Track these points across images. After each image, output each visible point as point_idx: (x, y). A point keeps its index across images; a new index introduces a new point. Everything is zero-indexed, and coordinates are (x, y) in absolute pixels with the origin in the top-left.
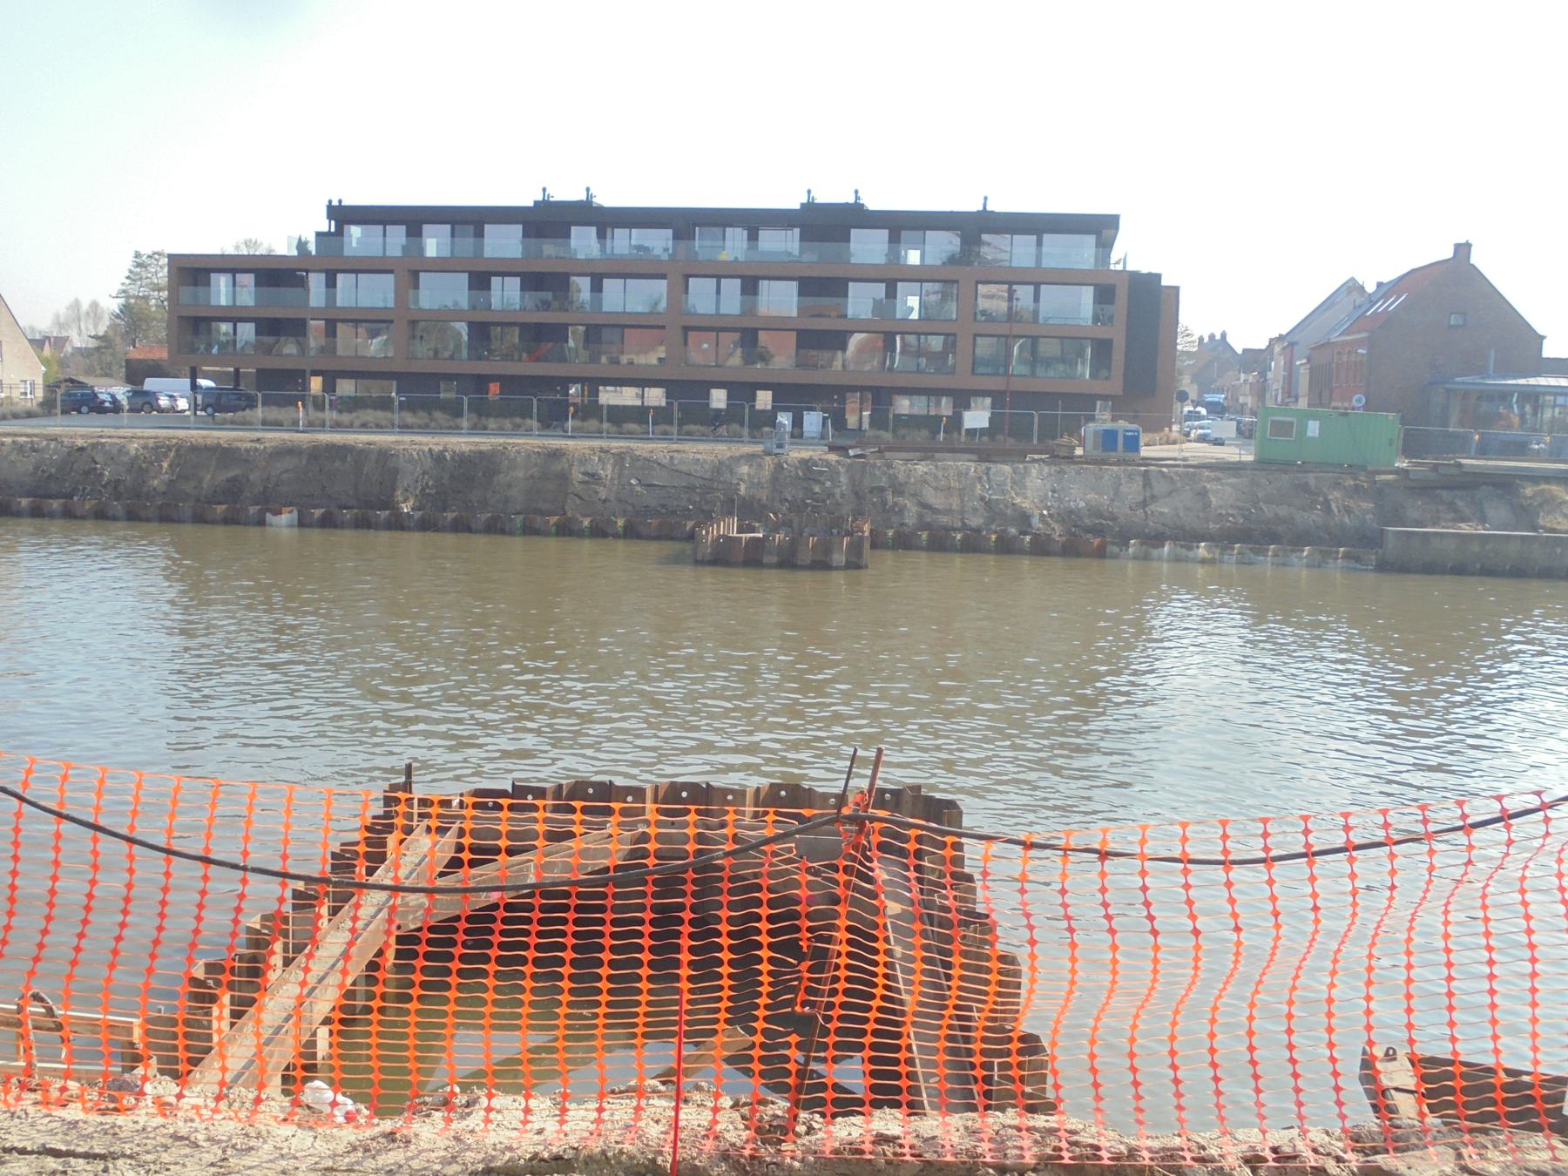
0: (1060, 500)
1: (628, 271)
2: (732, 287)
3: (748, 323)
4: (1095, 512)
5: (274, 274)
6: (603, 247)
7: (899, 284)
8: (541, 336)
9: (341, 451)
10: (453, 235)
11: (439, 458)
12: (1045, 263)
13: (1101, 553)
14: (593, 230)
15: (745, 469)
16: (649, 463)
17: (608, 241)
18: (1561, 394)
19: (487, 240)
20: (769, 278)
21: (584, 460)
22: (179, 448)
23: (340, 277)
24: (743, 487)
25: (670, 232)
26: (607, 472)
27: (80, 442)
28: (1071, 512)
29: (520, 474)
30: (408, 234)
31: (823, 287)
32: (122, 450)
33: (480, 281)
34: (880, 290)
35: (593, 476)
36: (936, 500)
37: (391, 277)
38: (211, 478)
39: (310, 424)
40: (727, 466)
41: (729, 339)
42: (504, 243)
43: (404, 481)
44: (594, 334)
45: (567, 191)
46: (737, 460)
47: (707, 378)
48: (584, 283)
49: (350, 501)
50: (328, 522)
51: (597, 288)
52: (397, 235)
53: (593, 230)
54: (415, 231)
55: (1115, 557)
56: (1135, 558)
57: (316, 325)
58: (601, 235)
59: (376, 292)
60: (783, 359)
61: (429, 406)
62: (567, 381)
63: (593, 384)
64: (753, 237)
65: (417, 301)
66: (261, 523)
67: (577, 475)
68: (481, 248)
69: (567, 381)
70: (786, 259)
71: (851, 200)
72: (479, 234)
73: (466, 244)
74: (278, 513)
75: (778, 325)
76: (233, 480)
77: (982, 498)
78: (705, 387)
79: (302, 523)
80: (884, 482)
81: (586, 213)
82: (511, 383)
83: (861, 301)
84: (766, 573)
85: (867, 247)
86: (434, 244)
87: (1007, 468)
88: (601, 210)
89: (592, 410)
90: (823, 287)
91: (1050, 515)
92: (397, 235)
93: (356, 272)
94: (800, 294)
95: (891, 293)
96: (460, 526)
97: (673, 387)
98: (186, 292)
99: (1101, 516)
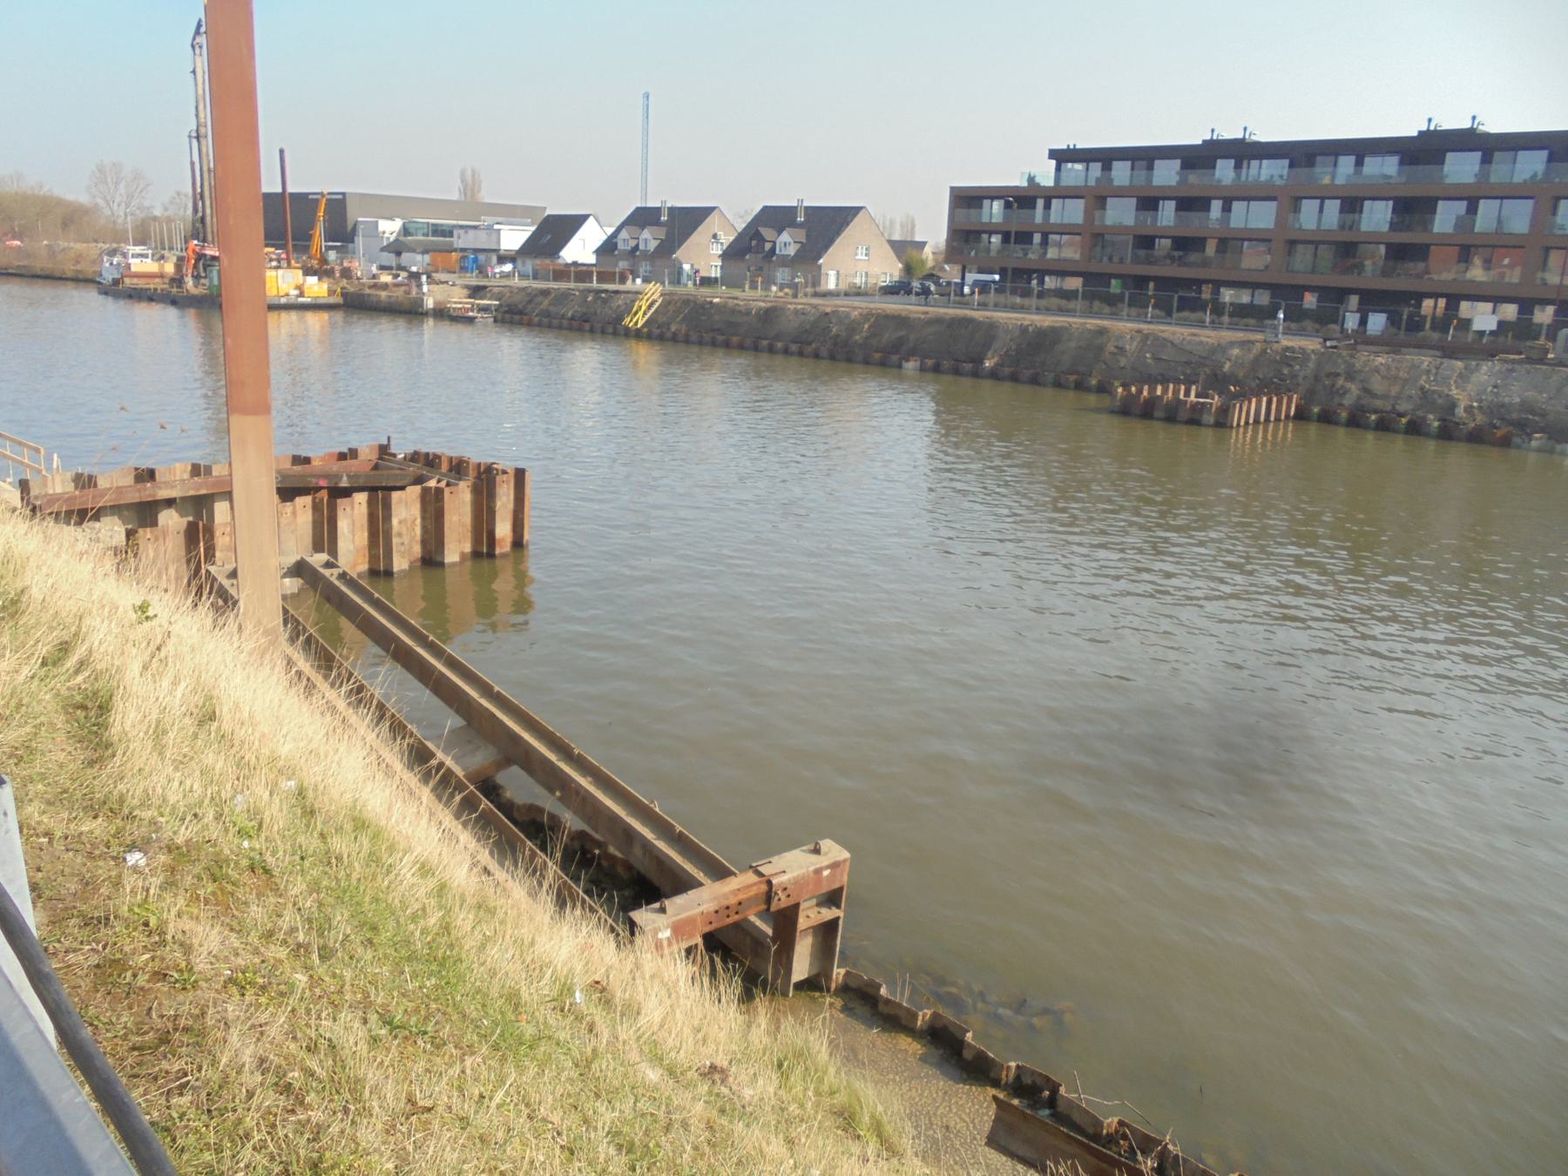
0: (1497, 395)
1: (1253, 195)
2: (1333, 207)
3: (1347, 237)
4: (1526, 407)
5: (1022, 199)
6: (1238, 175)
7: (1440, 203)
8: (1186, 244)
9: (969, 321)
10: (1133, 168)
11: (1024, 330)
12: (1063, 183)
13: (1505, 442)
14: (1232, 162)
15: (1236, 351)
16: (1162, 343)
17: (1244, 171)
18: (1051, 273)
19: (1156, 172)
20: (1374, 199)
21: (1120, 337)
22: (878, 315)
23: (1054, 202)
24: (1227, 366)
25: (1286, 162)
26: (1131, 347)
27: (828, 310)
28: (1503, 406)
29: (1073, 344)
30: (1103, 169)
31: (1413, 209)
32: (847, 315)
33: (1148, 203)
34: (1461, 207)
35: (1121, 349)
36: (1377, 385)
37: (1274, 204)
38: (888, 336)
39: (996, 305)
40: (1221, 349)
41: (1326, 253)
42: (1166, 174)
43: (996, 345)
44: (1224, 244)
45: (1453, 119)
46: (1232, 344)
47: (1301, 282)
48: (1216, 205)
49: (1033, 366)
50: (937, 369)
51: (1227, 208)
52: (1096, 169)
53: (1232, 162)
54: (1107, 167)
55: (1519, 447)
56: (1539, 450)
57: (1037, 238)
58: (1238, 166)
59: (1261, 216)
60: (1372, 264)
61: (1185, 304)
62: (1199, 283)
63: (1217, 284)
64: (1359, 163)
65: (1103, 218)
66: (900, 366)
67: (1111, 348)
68: (1149, 179)
69: (1420, 297)
70: (1381, 181)
71: (1467, 125)
72: (1150, 167)
73: (1141, 175)
74: (908, 361)
75: (1373, 239)
76: (900, 338)
77: (1422, 388)
78: (1298, 291)
79: (922, 369)
80: (1341, 369)
81: (1468, 140)
82: (1164, 283)
83: (1445, 218)
84: (1155, 423)
85: (1461, 168)
86: (1121, 173)
87: (1459, 364)
88: (1488, 136)
89: (1218, 309)
90: (1413, 209)
91: (1480, 408)
92: (1096, 169)
93: (1064, 197)
94: (1341, 211)
95: (1472, 209)
96: (1035, 381)
97: (1088, 277)
98: (962, 213)
99: (1532, 412)
